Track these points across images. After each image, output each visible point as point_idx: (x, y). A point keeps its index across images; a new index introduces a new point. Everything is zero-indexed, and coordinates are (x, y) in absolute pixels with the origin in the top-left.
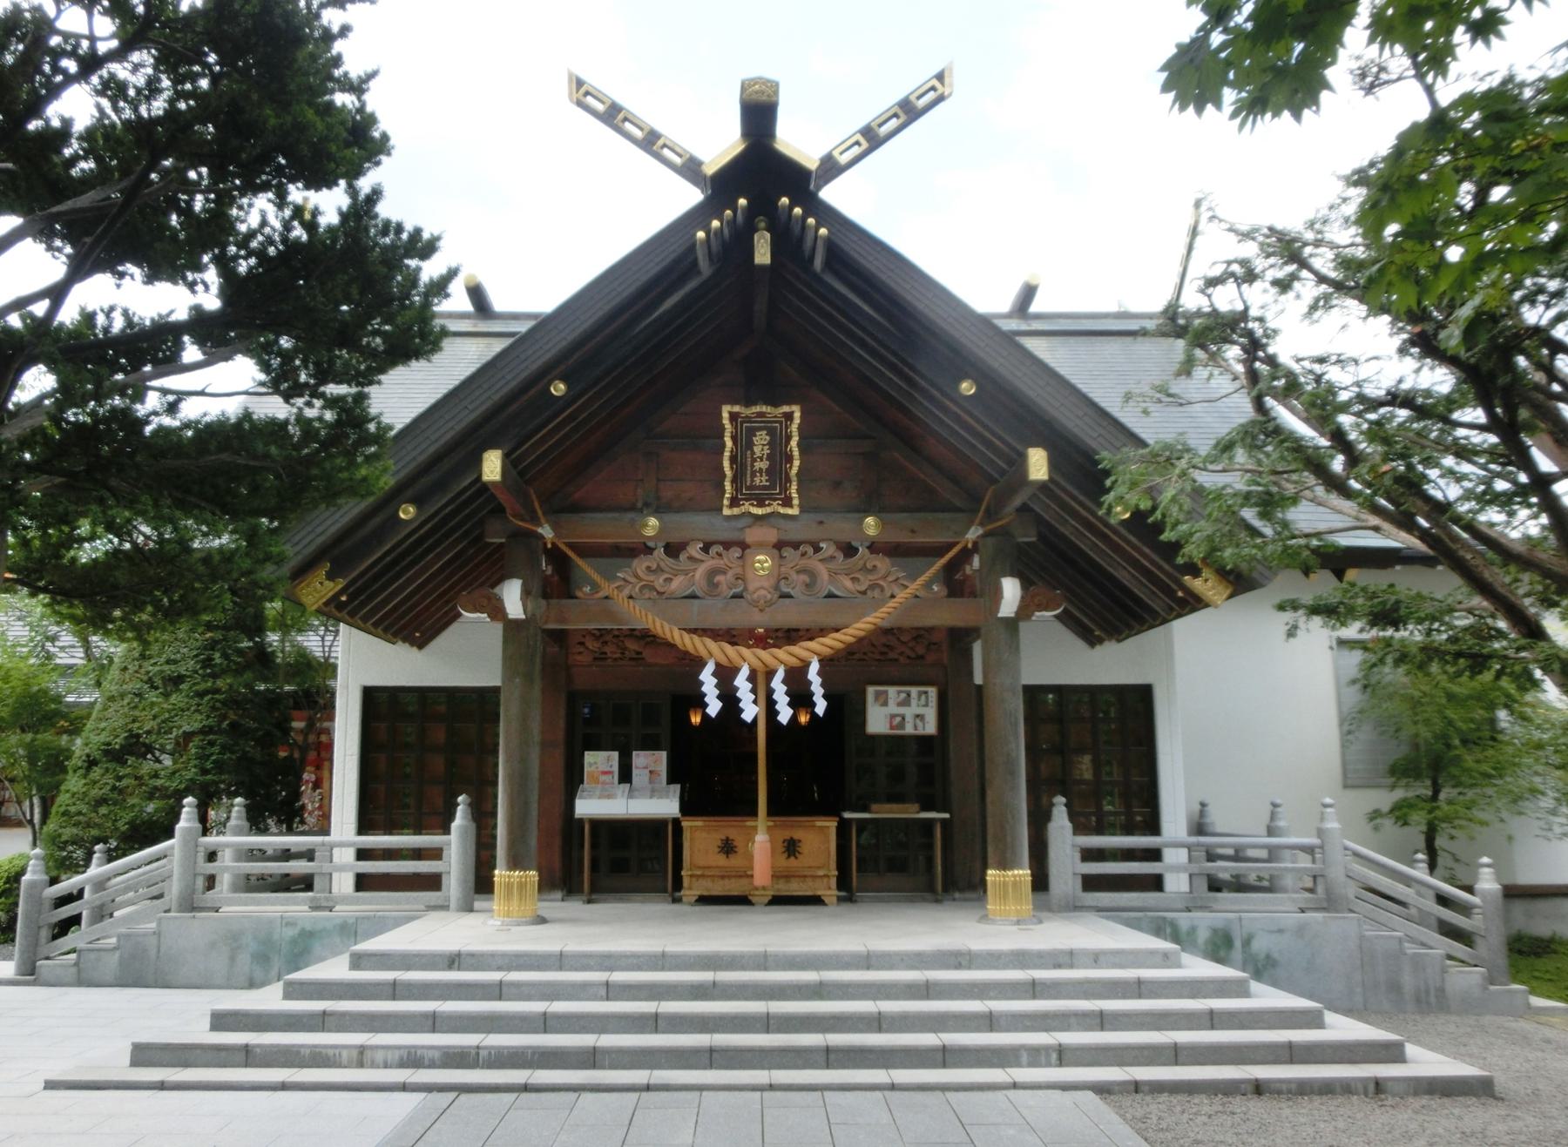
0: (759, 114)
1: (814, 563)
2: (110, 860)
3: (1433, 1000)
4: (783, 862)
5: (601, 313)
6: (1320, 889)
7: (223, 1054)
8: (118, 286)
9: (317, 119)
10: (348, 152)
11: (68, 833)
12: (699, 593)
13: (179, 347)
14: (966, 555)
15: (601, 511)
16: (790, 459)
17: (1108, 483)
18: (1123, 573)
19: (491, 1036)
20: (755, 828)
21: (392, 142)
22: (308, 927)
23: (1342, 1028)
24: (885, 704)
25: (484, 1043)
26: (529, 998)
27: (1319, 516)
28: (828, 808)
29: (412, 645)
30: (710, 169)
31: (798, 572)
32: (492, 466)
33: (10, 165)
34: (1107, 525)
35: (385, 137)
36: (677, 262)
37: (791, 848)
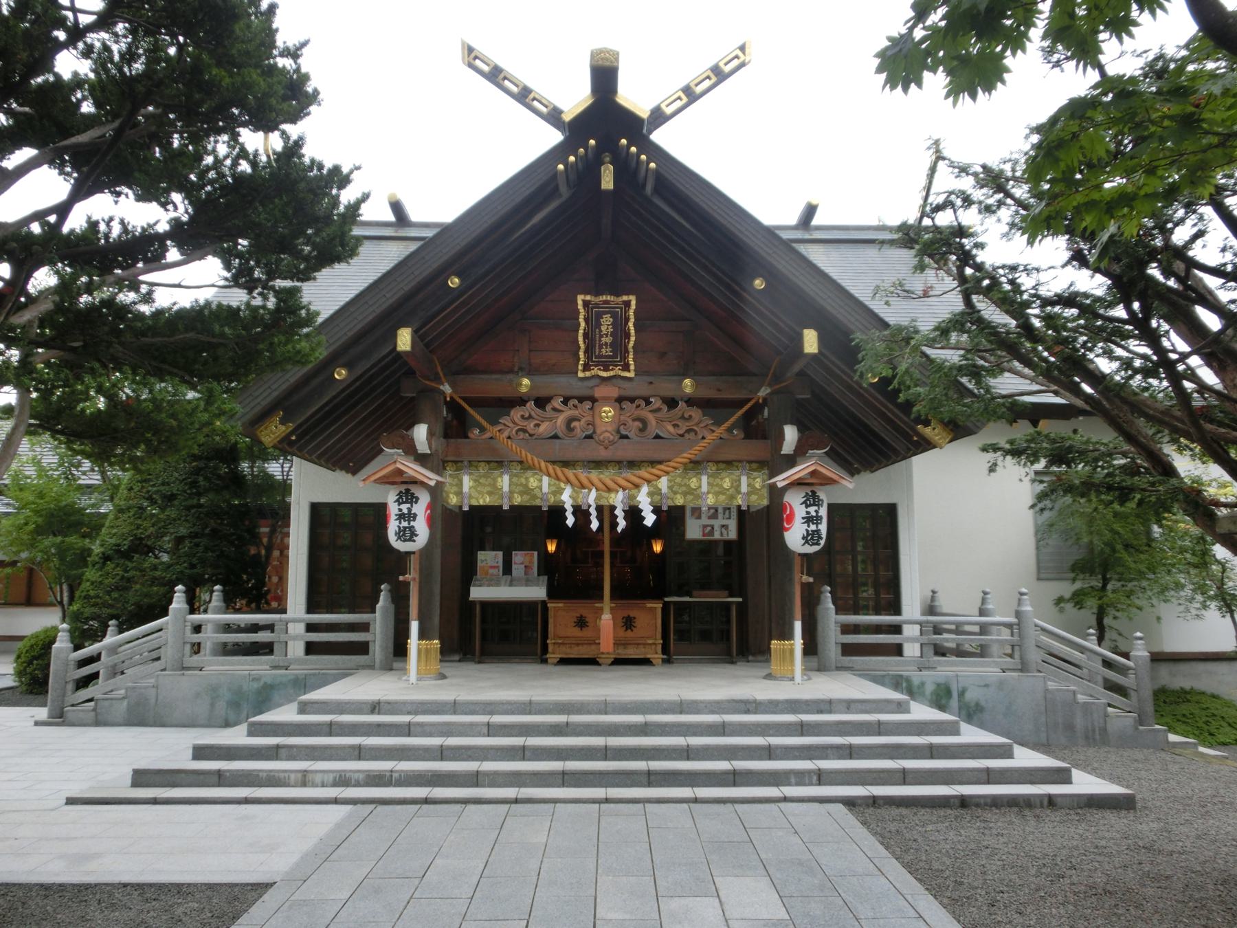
0: (604, 77)
1: (645, 413)
2: (121, 632)
3: (1098, 737)
4: (622, 633)
5: (486, 225)
6: (1017, 655)
7: (202, 777)
8: (116, 202)
9: (261, 80)
10: (285, 106)
11: (88, 611)
12: (560, 434)
13: (165, 249)
14: (758, 408)
15: (493, 372)
16: (628, 336)
17: (860, 356)
18: (874, 418)
19: (402, 763)
20: (602, 609)
21: (320, 97)
22: (269, 681)
23: (1026, 758)
24: (699, 517)
25: (397, 768)
26: (430, 735)
27: (1011, 383)
28: (657, 594)
29: (347, 472)
30: (567, 117)
31: (634, 420)
32: (404, 339)
33: (27, 109)
34: (861, 387)
35: (316, 92)
36: (541, 189)
37: (629, 623)
